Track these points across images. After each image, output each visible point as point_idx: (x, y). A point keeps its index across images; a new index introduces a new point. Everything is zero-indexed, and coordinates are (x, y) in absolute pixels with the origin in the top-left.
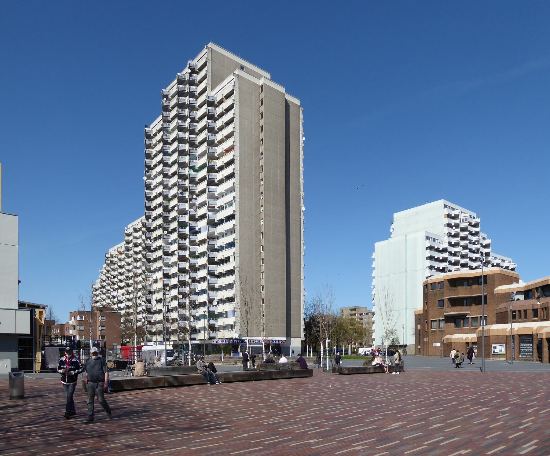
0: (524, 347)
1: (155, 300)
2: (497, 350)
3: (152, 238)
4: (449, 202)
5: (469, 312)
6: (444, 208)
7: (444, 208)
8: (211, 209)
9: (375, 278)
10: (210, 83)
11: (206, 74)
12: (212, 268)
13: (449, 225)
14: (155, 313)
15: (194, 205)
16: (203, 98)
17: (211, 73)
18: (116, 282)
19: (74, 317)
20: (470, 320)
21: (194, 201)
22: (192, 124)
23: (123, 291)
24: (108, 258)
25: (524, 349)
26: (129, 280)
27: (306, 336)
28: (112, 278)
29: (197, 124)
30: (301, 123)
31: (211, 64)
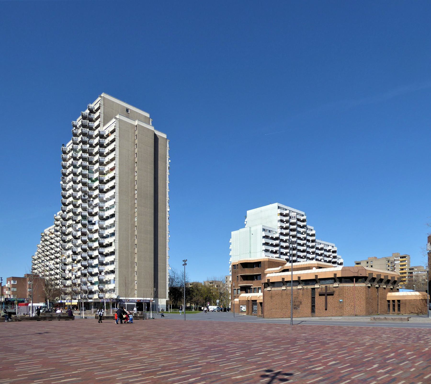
0: (255, 308)
1: (68, 270)
2: (242, 309)
3: (66, 226)
4: (282, 205)
5: (252, 285)
6: (278, 209)
7: (278, 209)
8: (101, 209)
9: (232, 256)
10: (103, 121)
11: (99, 115)
12: (101, 250)
13: (282, 221)
14: (68, 279)
15: (92, 205)
16: (96, 132)
17: (104, 114)
18: (49, 254)
19: (9, 281)
20: (253, 289)
21: (92, 202)
22: (90, 148)
23: (53, 262)
24: (43, 236)
25: (255, 309)
26: (57, 254)
27: (170, 296)
28: (46, 252)
29: (94, 149)
30: (168, 150)
31: (104, 108)
